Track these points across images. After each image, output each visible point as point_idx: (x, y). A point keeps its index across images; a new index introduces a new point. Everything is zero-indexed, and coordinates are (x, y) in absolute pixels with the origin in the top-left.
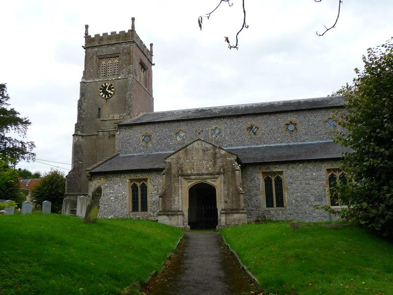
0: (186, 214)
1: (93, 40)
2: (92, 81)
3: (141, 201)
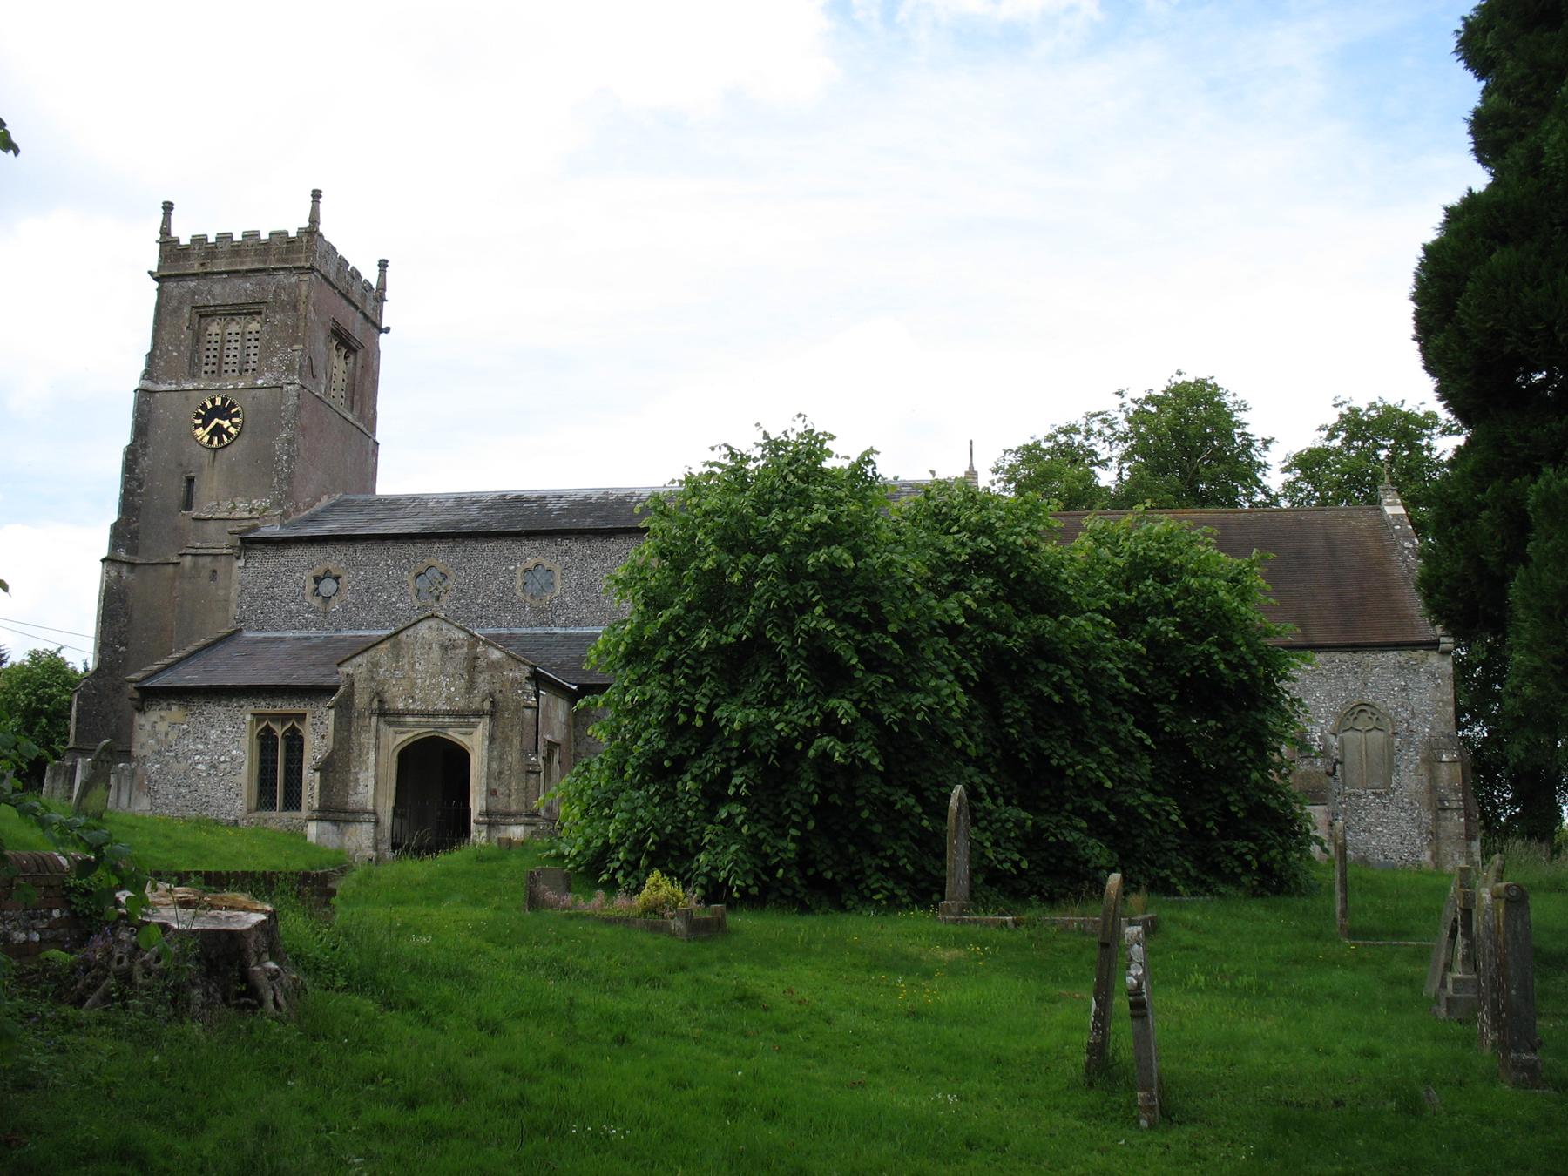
0: (387, 819)
1: (184, 252)
2: (174, 387)
3: (286, 778)
